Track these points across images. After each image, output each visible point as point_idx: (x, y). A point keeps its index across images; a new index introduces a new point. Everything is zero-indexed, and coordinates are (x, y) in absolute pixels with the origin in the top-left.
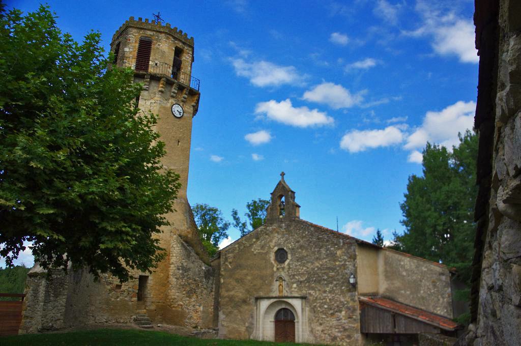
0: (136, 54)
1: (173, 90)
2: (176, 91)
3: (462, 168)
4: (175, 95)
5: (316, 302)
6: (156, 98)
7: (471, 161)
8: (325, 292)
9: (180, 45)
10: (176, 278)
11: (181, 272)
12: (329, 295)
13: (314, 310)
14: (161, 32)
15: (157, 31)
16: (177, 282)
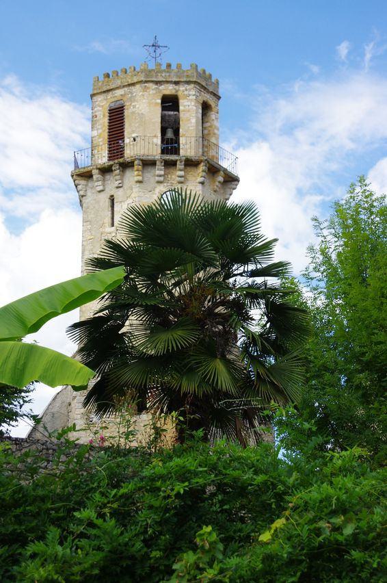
0: (106, 135)
1: (158, 172)
2: (162, 173)
3: (163, 568)
4: (162, 179)
6: (133, 195)
7: (161, 493)
9: (169, 89)
14: (133, 84)
15: (129, 85)
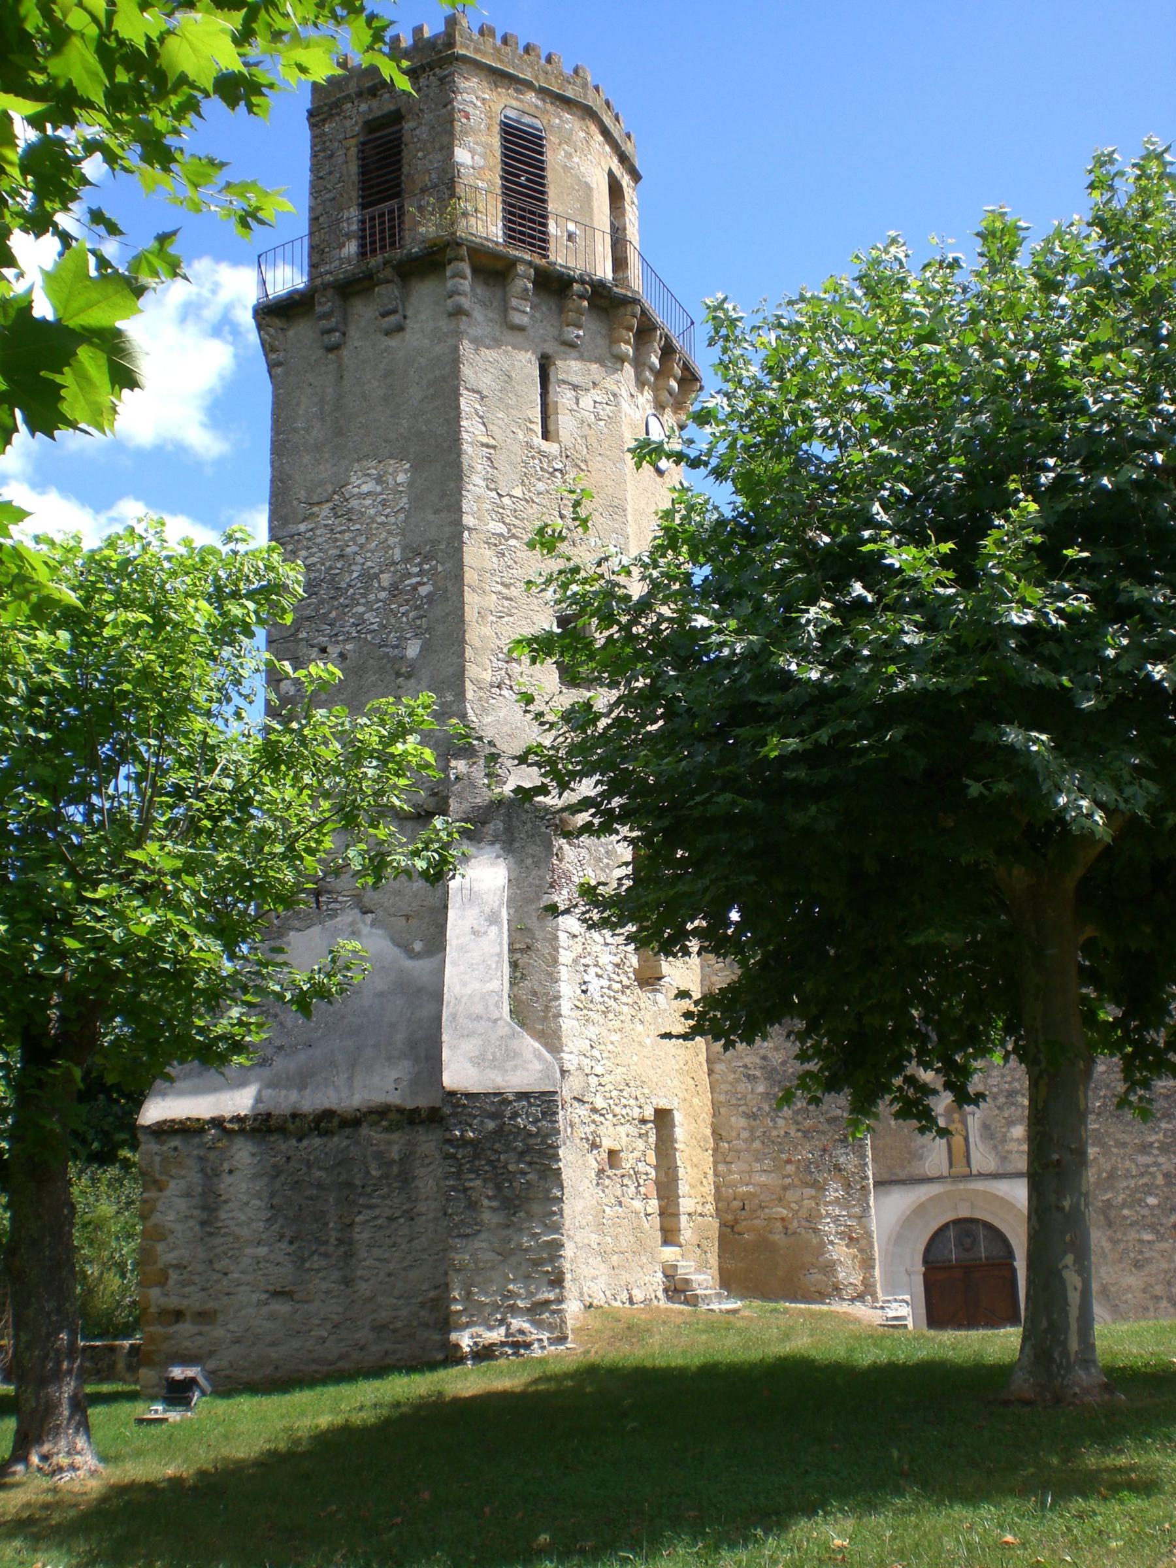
5: (1112, 1188)
8: (1144, 1148)
10: (746, 1115)
11: (761, 1089)
12: (1161, 1160)
13: (1107, 1218)
16: (752, 1130)
